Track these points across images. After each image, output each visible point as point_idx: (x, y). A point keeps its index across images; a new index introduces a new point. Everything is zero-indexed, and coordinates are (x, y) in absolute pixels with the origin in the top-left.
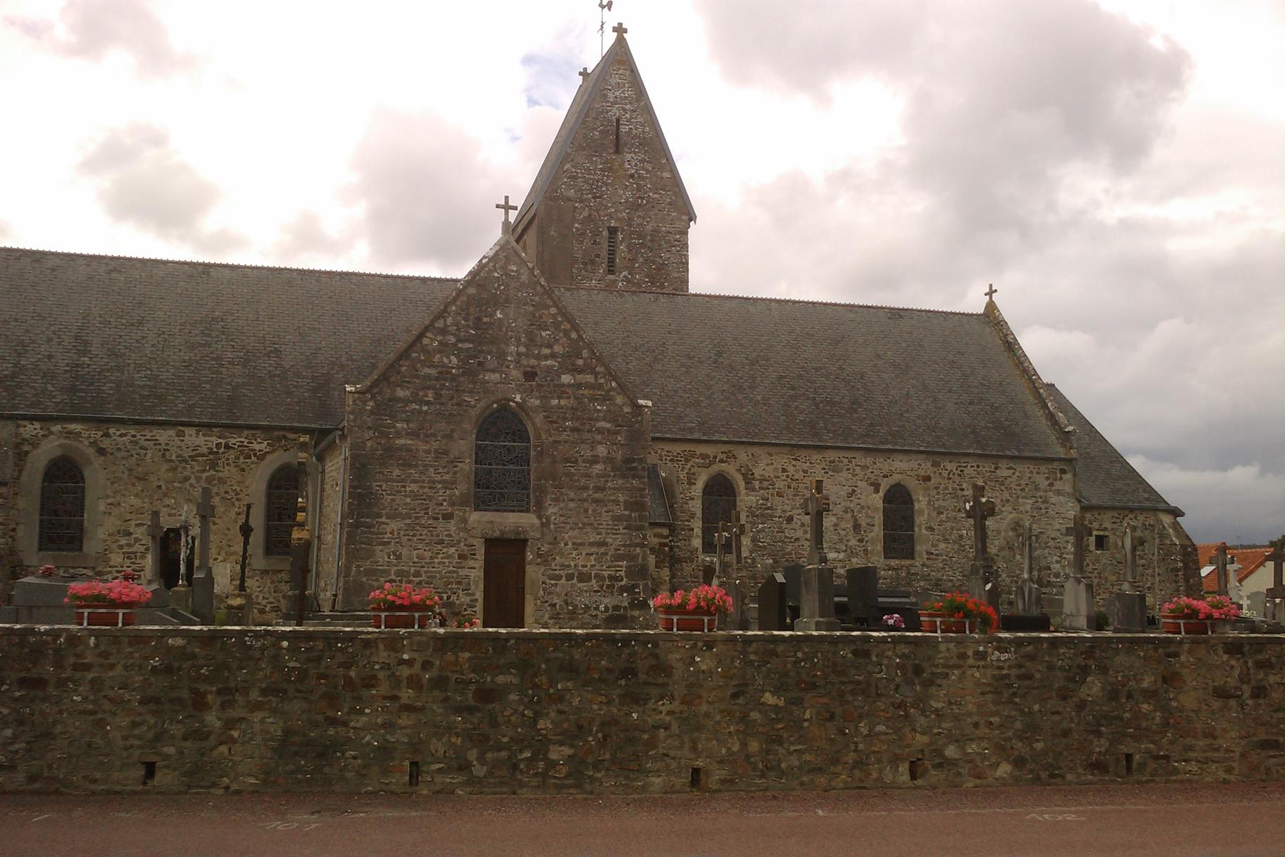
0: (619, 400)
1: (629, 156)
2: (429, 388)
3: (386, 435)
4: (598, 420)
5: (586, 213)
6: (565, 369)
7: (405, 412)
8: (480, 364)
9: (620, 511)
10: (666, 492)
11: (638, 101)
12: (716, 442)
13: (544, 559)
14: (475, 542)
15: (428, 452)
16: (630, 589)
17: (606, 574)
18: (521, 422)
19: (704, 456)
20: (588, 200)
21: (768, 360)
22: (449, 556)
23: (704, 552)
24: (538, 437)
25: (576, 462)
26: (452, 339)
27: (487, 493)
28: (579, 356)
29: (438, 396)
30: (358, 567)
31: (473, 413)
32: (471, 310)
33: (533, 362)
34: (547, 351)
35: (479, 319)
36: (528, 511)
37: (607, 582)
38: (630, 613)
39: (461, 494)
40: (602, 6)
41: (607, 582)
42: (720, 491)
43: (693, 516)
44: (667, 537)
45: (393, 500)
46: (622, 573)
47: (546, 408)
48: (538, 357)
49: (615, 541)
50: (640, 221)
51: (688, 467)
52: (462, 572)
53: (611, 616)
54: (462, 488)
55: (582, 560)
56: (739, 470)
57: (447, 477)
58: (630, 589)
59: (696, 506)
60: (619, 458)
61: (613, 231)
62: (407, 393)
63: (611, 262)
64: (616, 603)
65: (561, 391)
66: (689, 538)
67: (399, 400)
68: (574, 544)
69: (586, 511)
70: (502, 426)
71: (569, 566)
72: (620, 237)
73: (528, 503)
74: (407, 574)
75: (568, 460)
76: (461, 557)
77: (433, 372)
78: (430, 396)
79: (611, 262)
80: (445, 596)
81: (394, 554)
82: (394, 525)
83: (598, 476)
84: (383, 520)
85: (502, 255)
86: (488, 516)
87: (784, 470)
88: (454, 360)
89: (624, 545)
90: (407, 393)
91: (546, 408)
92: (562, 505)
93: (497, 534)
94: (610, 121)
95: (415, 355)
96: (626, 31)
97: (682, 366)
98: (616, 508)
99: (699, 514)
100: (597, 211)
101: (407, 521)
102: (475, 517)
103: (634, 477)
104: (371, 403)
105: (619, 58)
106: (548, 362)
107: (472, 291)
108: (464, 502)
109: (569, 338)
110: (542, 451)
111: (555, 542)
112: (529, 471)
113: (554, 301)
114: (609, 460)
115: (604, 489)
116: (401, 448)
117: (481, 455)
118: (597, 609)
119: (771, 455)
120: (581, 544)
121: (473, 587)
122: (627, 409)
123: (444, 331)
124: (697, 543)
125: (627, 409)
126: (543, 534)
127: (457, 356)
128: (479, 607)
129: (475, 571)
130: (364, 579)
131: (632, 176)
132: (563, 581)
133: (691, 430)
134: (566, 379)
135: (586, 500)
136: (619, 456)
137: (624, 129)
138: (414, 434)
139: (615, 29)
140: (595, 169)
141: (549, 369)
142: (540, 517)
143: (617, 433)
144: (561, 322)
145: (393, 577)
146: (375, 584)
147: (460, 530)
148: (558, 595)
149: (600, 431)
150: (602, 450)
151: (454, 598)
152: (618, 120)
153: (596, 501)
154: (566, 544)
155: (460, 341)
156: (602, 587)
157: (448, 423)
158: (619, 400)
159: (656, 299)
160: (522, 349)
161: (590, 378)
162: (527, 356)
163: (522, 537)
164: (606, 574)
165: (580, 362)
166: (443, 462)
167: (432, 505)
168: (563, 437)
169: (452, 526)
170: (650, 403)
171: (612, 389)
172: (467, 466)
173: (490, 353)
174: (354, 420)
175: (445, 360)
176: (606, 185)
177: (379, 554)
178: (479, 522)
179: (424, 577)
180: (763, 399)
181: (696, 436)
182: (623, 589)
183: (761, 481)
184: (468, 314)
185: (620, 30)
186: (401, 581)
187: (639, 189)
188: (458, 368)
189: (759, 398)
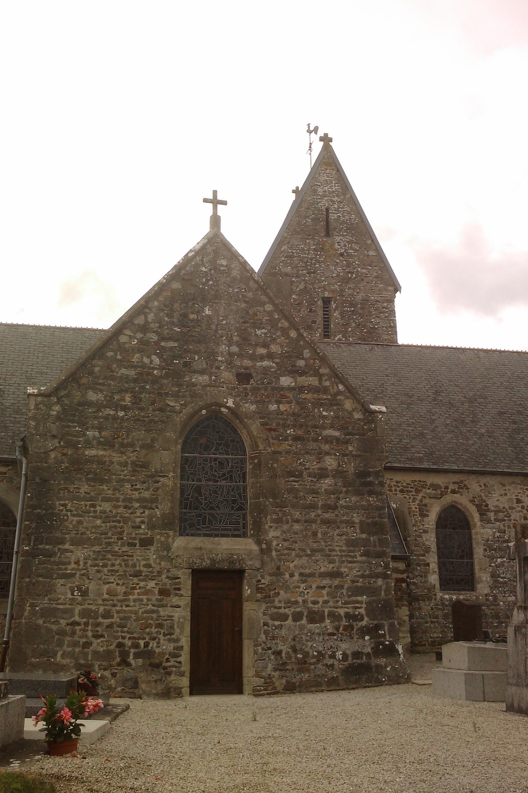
0: (348, 405)
1: (338, 239)
2: (126, 391)
3: (74, 446)
4: (324, 428)
5: (302, 286)
6: (283, 370)
7: (96, 418)
8: (186, 364)
9: (356, 534)
10: (399, 522)
11: (344, 194)
12: (446, 471)
13: (266, 595)
14: (179, 573)
15: (125, 464)
16: (372, 631)
17: (342, 612)
18: (235, 431)
19: (435, 487)
20: (304, 275)
21: (485, 398)
22: (147, 592)
23: (441, 589)
24: (255, 446)
25: (301, 475)
26: (154, 337)
27: (195, 514)
28: (300, 356)
29: (136, 400)
30: (33, 605)
31: (178, 419)
32: (176, 306)
33: (247, 362)
34: (262, 351)
35: (185, 316)
36: (244, 535)
37: (344, 622)
38: (375, 661)
39: (163, 515)
40: (310, 132)
41: (344, 622)
42: (454, 524)
43: (427, 550)
44: (403, 572)
45: (80, 522)
46: (363, 611)
47: (263, 414)
48: (253, 358)
49: (352, 571)
50: (350, 292)
51: (419, 498)
52: (163, 612)
53: (351, 666)
54: (164, 507)
55: (311, 595)
56: (472, 501)
57: (146, 495)
58: (372, 631)
59: (430, 539)
60: (351, 470)
61: (327, 302)
62: (101, 397)
63: (326, 327)
64: (356, 648)
65: (280, 395)
66: (425, 574)
67: (90, 404)
68: (301, 574)
69: (315, 534)
70: (212, 433)
71: (297, 602)
72: (334, 306)
73: (245, 526)
74: (96, 615)
75: (291, 474)
76: (164, 592)
77: (132, 373)
78: (128, 399)
79: (326, 327)
80: (142, 643)
81: (79, 589)
82: (80, 553)
83: (328, 492)
84: (67, 546)
85: (210, 249)
86: (197, 542)
87: (519, 501)
88: (156, 360)
89: (362, 576)
90: (101, 397)
91: (263, 414)
92: (285, 527)
93: (207, 563)
94: (319, 210)
95: (110, 354)
96: (331, 140)
97: (402, 403)
98: (350, 530)
99: (434, 548)
100: (313, 284)
101: (97, 548)
102: (179, 543)
103: (370, 493)
104: (57, 408)
105: (328, 164)
106: (265, 363)
107: (176, 285)
108: (166, 523)
109: (288, 337)
110: (259, 464)
111: (278, 572)
112: (245, 488)
113: (270, 298)
114: (339, 473)
115: (335, 508)
116: (90, 460)
117: (186, 467)
118: (333, 656)
119: (504, 485)
120: (312, 575)
121: (177, 631)
122: (357, 416)
123: (144, 329)
124: (434, 579)
125: (357, 416)
126: (263, 563)
127: (160, 356)
128: (185, 657)
129: (180, 610)
130: (40, 622)
131: (342, 255)
132: (290, 621)
133: (420, 460)
134: (286, 381)
135: (314, 521)
136: (351, 468)
137: (333, 217)
138: (108, 444)
139: (321, 139)
140: (309, 250)
141: (265, 371)
142: (259, 542)
143: (347, 442)
144: (279, 320)
145: (77, 618)
146: (54, 627)
147: (162, 558)
148: (284, 640)
149: (328, 440)
150: (330, 462)
151: (153, 644)
152: (327, 210)
153: (326, 522)
154: (292, 575)
155: (164, 339)
156: (337, 629)
157: (148, 431)
158: (348, 405)
159: (371, 350)
160: (235, 349)
161: (313, 381)
162: (241, 356)
163: (237, 566)
164: (342, 612)
165: (301, 363)
166: (141, 477)
167: (127, 529)
168: (285, 446)
169: (152, 554)
170: (384, 409)
171: (339, 393)
172: (170, 481)
173: (197, 352)
174: (36, 427)
175: (146, 360)
176: (319, 262)
177: (59, 589)
178: (185, 549)
179: (116, 619)
180: (488, 432)
181: (425, 465)
182: (363, 631)
183: (496, 512)
184: (172, 310)
185: (326, 140)
186: (86, 624)
187: (348, 265)
188: (161, 368)
189: (483, 431)
